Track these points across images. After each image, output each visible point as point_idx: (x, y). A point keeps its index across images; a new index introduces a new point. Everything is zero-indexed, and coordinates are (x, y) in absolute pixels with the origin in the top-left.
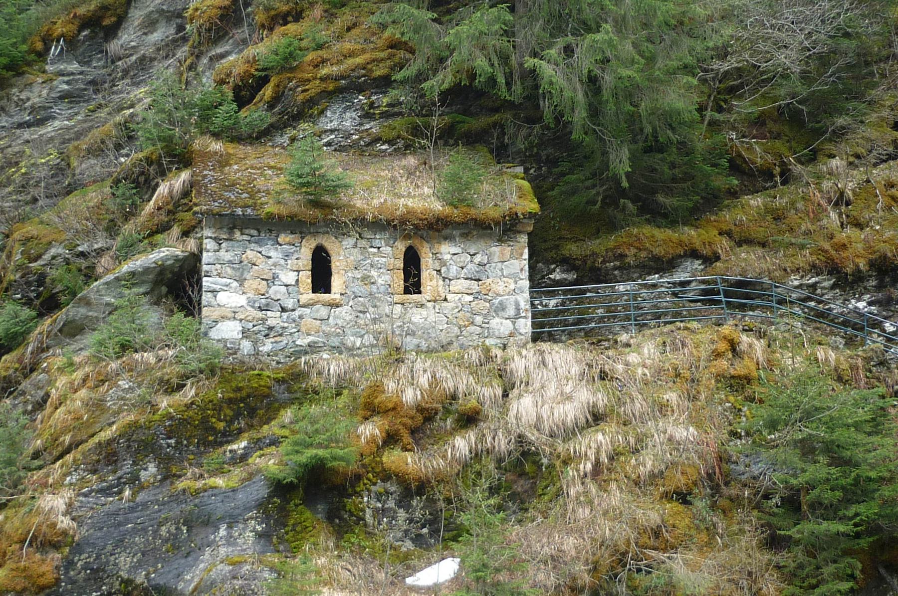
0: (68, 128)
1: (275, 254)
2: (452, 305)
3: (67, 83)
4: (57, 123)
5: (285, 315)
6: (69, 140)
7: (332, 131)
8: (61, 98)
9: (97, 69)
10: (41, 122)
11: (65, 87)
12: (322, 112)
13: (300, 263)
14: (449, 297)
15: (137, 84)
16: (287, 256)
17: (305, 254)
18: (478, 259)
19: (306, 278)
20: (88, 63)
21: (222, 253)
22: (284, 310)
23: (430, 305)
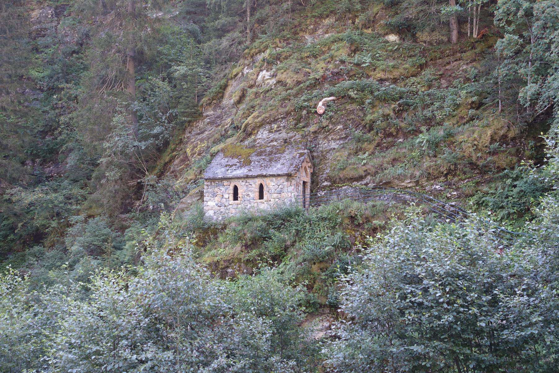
0: (210, 134)
1: (223, 189)
8: (208, 124)
9: (219, 111)
16: (226, 189)
17: (231, 188)
18: (280, 187)
19: (257, 194)
20: (216, 111)
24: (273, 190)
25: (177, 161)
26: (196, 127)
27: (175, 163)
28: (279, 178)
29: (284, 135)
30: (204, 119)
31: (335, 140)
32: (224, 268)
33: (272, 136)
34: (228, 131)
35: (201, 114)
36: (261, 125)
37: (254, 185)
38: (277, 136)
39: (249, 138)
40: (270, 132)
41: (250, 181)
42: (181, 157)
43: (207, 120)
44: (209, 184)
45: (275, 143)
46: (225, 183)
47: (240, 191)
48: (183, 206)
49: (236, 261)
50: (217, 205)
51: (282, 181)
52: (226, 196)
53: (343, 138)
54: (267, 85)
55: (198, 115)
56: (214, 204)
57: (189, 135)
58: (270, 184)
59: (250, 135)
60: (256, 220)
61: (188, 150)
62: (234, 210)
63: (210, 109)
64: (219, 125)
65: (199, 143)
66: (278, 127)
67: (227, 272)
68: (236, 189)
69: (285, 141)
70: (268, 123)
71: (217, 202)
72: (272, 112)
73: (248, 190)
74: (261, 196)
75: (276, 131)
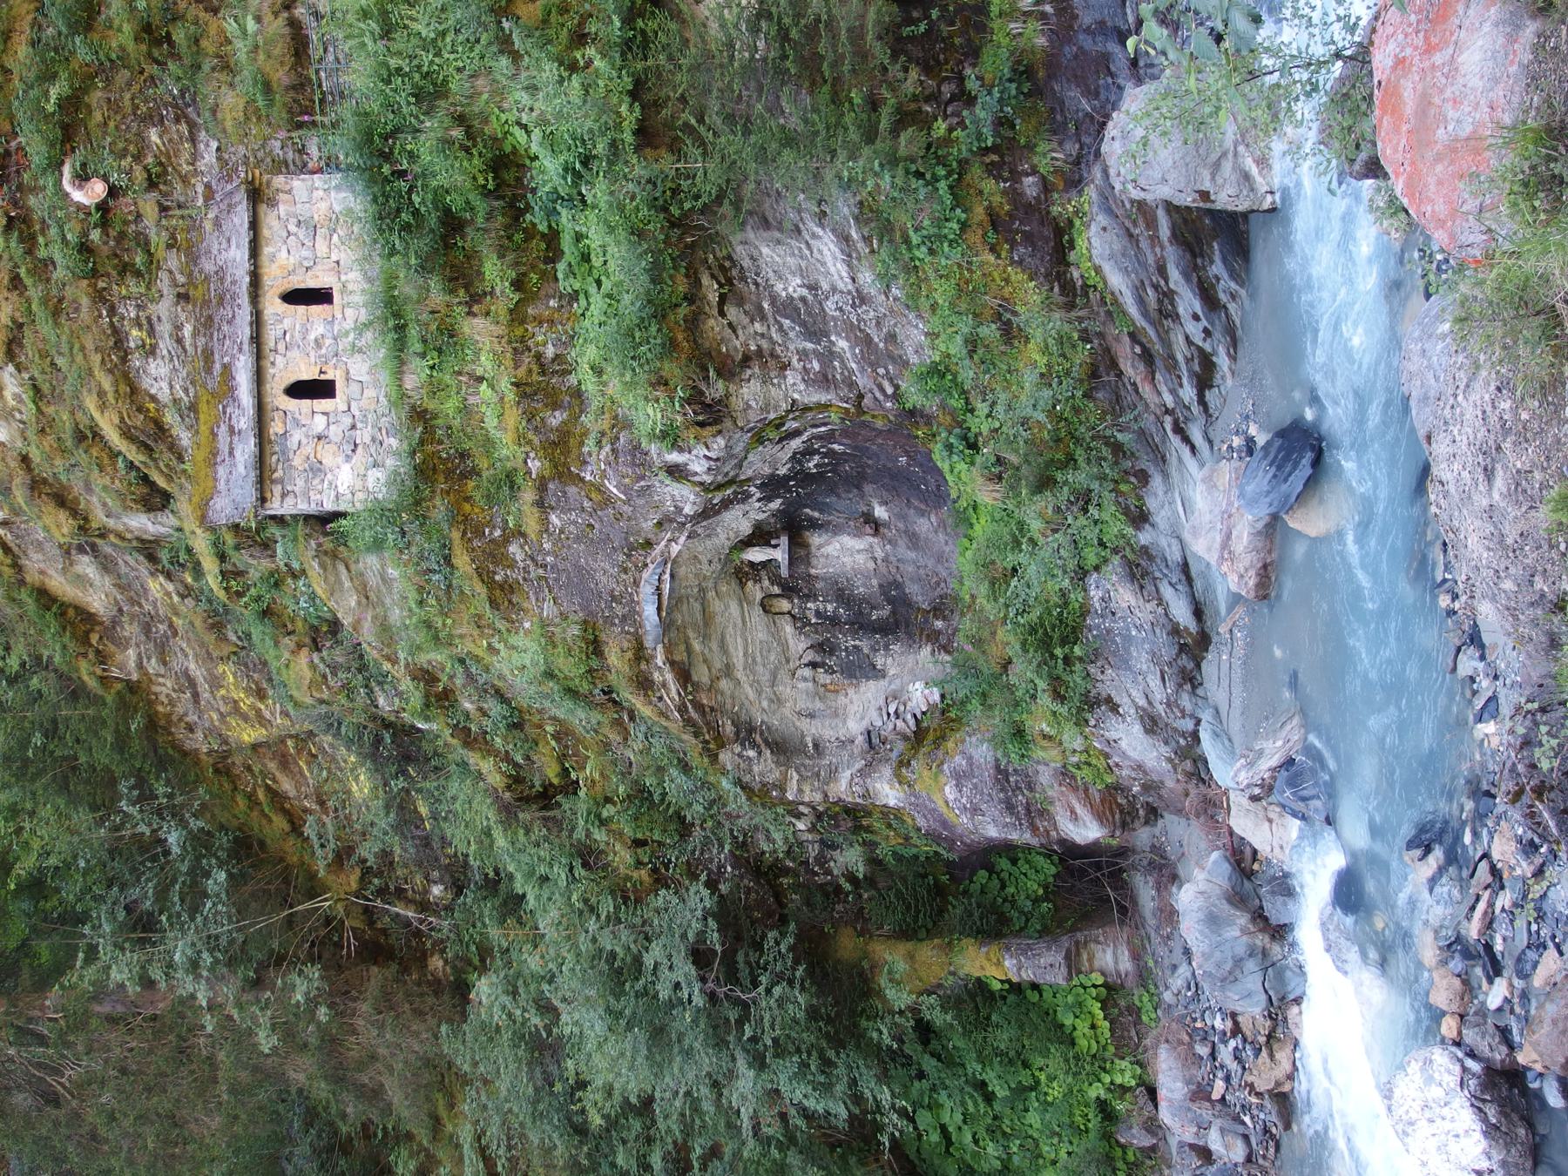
0: (196, 655)
1: (296, 436)
2: (343, 255)
3: (149, 659)
4: (192, 666)
5: (359, 425)
6: (208, 653)
7: (171, 387)
8: (165, 663)
9: (130, 630)
10: (192, 683)
11: (153, 660)
12: (153, 398)
13: (304, 411)
14: (334, 258)
15: (146, 590)
16: (297, 424)
17: (292, 405)
20: (128, 640)
21: (296, 489)
22: (353, 427)
23: (343, 278)
24: (305, 253)
25: (287, 785)
26: (172, 703)
27: (292, 793)
28: (266, 232)
29: (163, 309)
30: (146, 674)
31: (195, 157)
32: (542, 365)
33: (165, 345)
34: (186, 586)
35: (132, 687)
36: (132, 391)
37: (287, 324)
38: (164, 329)
39: (174, 432)
40: (151, 352)
41: (271, 335)
42: (272, 766)
43: (153, 666)
44: (277, 489)
45: (187, 331)
46: (276, 428)
47: (307, 373)
48: (367, 625)
49: (519, 332)
50: (348, 458)
51: (275, 223)
52: (320, 423)
53: (190, 132)
54: (21, 401)
55: (135, 693)
56: (346, 468)
57: (199, 735)
58: (286, 263)
59: (161, 430)
60: (390, 282)
61: (249, 735)
62: (364, 379)
63: (119, 657)
64: (171, 625)
65: (223, 692)
66: (140, 326)
67: (557, 357)
68: (299, 390)
69: (183, 297)
70: (124, 360)
71: (340, 459)
72: (90, 345)
73: (300, 346)
74: (320, 296)
75: (152, 332)
